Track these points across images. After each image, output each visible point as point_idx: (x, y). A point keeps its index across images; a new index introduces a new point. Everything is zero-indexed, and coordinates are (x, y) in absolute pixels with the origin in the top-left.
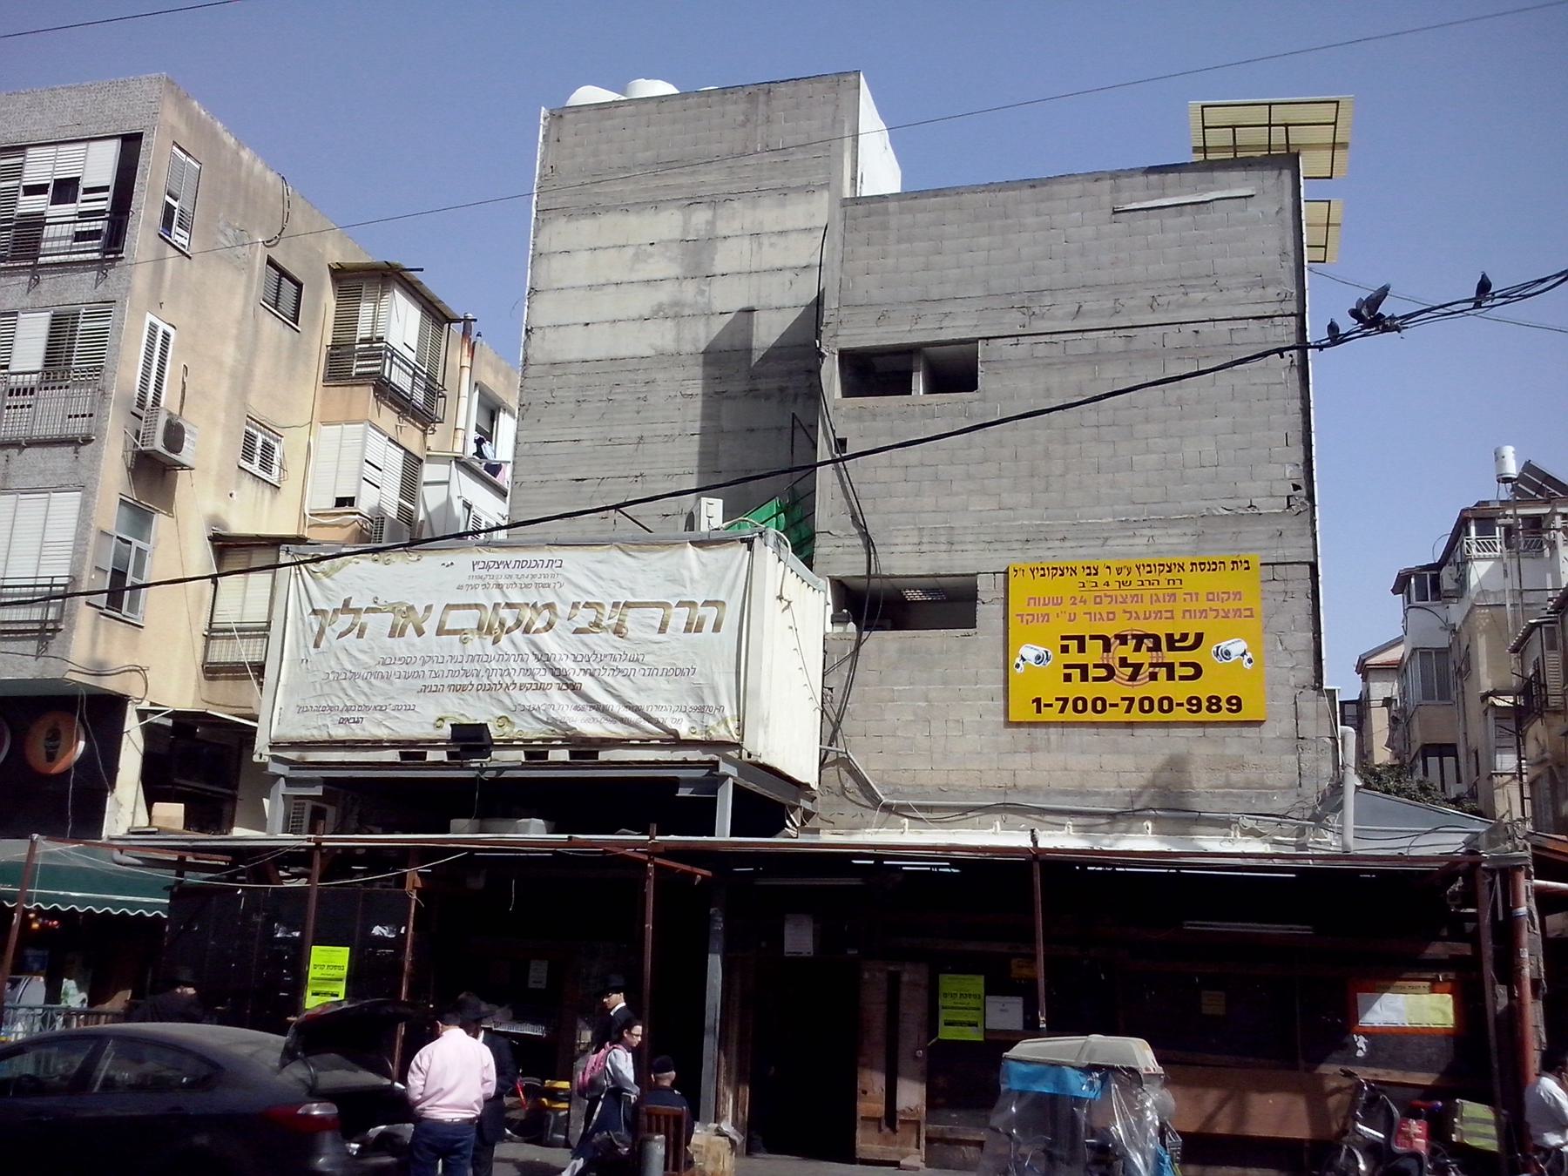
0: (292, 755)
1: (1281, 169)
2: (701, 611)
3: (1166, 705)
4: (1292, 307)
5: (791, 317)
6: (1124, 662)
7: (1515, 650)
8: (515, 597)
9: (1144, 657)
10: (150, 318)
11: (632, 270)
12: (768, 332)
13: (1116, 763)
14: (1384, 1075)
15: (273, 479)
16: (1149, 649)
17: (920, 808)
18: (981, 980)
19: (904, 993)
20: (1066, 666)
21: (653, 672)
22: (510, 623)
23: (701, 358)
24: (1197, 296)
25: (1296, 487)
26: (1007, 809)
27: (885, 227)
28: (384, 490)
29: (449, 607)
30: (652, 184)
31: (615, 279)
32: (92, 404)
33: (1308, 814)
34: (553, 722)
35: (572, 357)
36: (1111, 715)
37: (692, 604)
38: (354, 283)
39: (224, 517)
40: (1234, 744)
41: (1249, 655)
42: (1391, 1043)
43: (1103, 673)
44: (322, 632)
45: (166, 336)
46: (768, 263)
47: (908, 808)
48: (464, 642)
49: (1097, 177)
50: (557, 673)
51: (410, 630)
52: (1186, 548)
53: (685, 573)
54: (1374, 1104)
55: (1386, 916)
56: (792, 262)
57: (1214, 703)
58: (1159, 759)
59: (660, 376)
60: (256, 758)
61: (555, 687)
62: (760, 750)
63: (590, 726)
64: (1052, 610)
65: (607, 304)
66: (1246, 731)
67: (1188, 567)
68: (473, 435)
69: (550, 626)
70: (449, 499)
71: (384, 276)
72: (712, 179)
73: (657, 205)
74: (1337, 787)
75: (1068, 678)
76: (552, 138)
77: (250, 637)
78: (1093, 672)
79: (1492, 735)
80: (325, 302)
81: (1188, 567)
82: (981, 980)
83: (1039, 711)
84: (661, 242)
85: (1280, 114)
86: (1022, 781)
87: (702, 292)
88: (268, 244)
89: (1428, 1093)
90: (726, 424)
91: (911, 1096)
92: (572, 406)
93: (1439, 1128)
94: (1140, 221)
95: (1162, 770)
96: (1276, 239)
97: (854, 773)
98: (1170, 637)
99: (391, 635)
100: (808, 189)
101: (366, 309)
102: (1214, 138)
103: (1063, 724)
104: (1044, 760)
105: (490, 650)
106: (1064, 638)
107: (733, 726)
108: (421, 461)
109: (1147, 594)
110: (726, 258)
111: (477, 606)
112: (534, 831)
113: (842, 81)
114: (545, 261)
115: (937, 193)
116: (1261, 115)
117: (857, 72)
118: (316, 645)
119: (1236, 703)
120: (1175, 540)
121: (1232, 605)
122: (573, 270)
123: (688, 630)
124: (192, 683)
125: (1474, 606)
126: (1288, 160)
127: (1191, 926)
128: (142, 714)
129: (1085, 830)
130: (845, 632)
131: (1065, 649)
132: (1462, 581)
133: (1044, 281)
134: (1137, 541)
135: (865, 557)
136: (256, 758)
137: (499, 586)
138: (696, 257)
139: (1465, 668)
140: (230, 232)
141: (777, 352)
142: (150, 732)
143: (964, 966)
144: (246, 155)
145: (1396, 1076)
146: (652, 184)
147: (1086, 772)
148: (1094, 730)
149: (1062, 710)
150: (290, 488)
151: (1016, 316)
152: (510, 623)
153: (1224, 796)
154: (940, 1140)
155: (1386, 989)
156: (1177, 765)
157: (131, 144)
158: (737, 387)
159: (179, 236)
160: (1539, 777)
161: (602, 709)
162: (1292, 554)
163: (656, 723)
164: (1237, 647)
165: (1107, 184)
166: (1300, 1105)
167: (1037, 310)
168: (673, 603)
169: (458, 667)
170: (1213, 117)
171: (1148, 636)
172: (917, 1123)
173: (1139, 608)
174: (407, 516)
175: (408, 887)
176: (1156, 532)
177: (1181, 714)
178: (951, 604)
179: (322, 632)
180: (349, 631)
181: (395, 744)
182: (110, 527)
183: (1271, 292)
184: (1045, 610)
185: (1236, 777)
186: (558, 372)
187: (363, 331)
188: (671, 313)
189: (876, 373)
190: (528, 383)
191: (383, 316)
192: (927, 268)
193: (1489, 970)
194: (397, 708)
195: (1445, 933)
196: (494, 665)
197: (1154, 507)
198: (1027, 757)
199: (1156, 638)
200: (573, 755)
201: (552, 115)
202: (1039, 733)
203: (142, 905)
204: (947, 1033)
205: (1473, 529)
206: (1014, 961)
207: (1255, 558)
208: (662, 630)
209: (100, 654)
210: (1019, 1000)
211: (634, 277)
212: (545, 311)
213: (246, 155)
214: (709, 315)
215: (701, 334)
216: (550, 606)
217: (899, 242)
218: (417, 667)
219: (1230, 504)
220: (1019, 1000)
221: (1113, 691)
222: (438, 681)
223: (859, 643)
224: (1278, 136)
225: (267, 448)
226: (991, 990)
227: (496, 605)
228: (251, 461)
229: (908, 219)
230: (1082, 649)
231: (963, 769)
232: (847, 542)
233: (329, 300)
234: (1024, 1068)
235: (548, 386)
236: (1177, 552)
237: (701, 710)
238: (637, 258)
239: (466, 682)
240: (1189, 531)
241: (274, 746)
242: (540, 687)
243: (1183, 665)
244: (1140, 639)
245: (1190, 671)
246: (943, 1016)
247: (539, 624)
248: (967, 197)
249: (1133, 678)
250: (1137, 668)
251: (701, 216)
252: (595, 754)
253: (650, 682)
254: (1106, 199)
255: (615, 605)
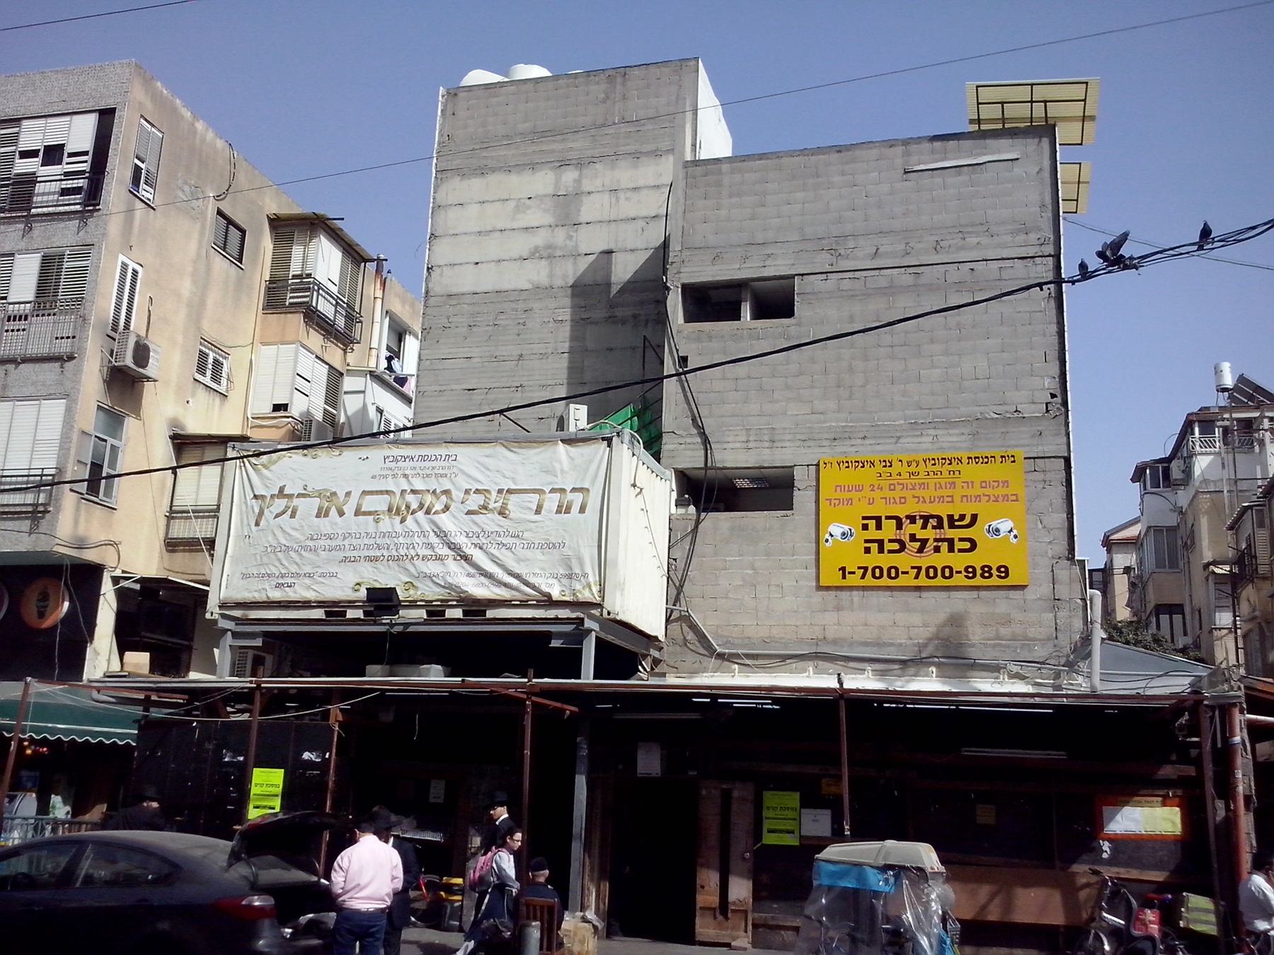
0: (237, 613)
1: (1040, 137)
2: (570, 496)
3: (947, 573)
4: (1050, 249)
5: (642, 257)
6: (913, 538)
7: (1231, 528)
8: (419, 485)
9: (930, 534)
10: (122, 258)
11: (513, 219)
12: (624, 270)
13: (906, 620)
14: (1125, 873)
15: (222, 389)
16: (934, 527)
17: (748, 656)
18: (797, 795)
19: (735, 807)
20: (866, 541)
21: (530, 546)
22: (414, 506)
23: (569, 291)
24: (973, 240)
25: (1053, 396)
26: (818, 657)
27: (719, 184)
28: (312, 398)
29: (365, 493)
30: (530, 149)
31: (499, 226)
32: (75, 328)
33: (1063, 661)
34: (449, 587)
35: (464, 290)
36: (902, 581)
37: (562, 491)
38: (287, 229)
39: (182, 419)
40: (1003, 604)
41: (1015, 532)
42: (1130, 847)
43: (896, 546)
44: (261, 513)
45: (135, 273)
46: (624, 213)
47: (737, 656)
48: (377, 521)
49: (891, 144)
50: (452, 546)
51: (333, 512)
52: (964, 445)
53: (557, 465)
54: (1116, 897)
55: (1126, 744)
56: (644, 213)
57: (986, 571)
58: (942, 616)
59: (536, 305)
60: (208, 616)
61: (451, 558)
62: (617, 609)
63: (479, 589)
64: (855, 495)
65: (493, 247)
66: (1012, 594)
67: (965, 461)
68: (384, 353)
69: (447, 508)
70: (365, 405)
71: (312, 224)
72: (578, 145)
73: (533, 167)
74: (1087, 639)
75: (867, 550)
76: (449, 112)
77: (203, 517)
78: (888, 546)
79: (1212, 597)
80: (264, 245)
81: (965, 461)
82: (797, 795)
83: (844, 577)
84: (537, 196)
85: (1040, 93)
86: (830, 634)
87: (570, 237)
88: (218, 198)
89: (1161, 887)
90: (590, 344)
91: (740, 890)
92: (465, 330)
93: (1169, 916)
94: (926, 180)
95: (944, 625)
96: (1037, 194)
97: (694, 627)
98: (950, 517)
99: (318, 516)
100: (657, 154)
101: (297, 251)
102: (986, 112)
103: (864, 588)
104: (848, 617)
105: (398, 528)
106: (864, 518)
107: (595, 589)
108: (342, 374)
109: (932, 483)
110: (590, 209)
111: (387, 492)
112: (434, 675)
113: (684, 66)
114: (442, 212)
115: (762, 156)
116: (1024, 93)
117: (696, 59)
118: (257, 524)
119: (1004, 571)
120: (954, 439)
121: (1001, 491)
122: (465, 219)
123: (559, 512)
124: (156, 555)
125: (1197, 492)
126: (1047, 130)
127: (968, 752)
128: (116, 580)
129: (882, 674)
130: (686, 514)
131: (865, 527)
132: (1188, 472)
133: (848, 229)
134: (924, 439)
135: (703, 452)
136: (208, 616)
137: (405, 476)
138: (566, 208)
139: (1191, 543)
140: (187, 188)
141: (632, 286)
142: (122, 595)
143: (784, 784)
144: (200, 126)
145: (1134, 874)
146: (530, 149)
147: (883, 627)
148: (889, 593)
149: (863, 577)
150: (236, 397)
151: (825, 257)
152: (414, 506)
153: (994, 646)
154: (763, 926)
155: (1126, 803)
156: (956, 621)
157: (106, 117)
158: (599, 314)
159: (145, 192)
160: (1250, 631)
161: (489, 576)
162: (1050, 449)
163: (533, 587)
164: (1005, 525)
165: (899, 150)
166: (1056, 897)
167: (842, 252)
168: (547, 490)
169: (372, 541)
170: (986, 95)
171: (933, 517)
172: (745, 912)
173: (926, 494)
174: (330, 419)
175: (332, 720)
176: (939, 432)
177: (959, 580)
178: (773, 490)
179: (261, 513)
180: (284, 512)
181: (321, 604)
182: (90, 428)
183: (1033, 237)
184: (849, 495)
185: (1004, 631)
186: (454, 302)
187: (295, 269)
188: (545, 254)
189: (712, 303)
190: (429, 311)
191: (311, 257)
192: (753, 218)
193: (1210, 788)
194: (323, 575)
195: (1174, 757)
196: (401, 540)
197: (938, 412)
198: (835, 614)
199: (939, 518)
200: (465, 613)
201: (448, 93)
202: (844, 595)
203: (116, 735)
204: (769, 839)
205: (1197, 430)
206: (824, 781)
207: (1020, 453)
208: (538, 512)
209: (81, 531)
210: (828, 812)
211: (515, 225)
212: (443, 252)
213: (200, 126)
214: (576, 256)
215: (570, 272)
216: (447, 492)
217: (730, 196)
218: (338, 542)
219: (999, 409)
220: (828, 812)
221: (904, 561)
222: (356, 553)
223: (698, 522)
224: (1039, 110)
225: (217, 364)
226: (805, 804)
227: (403, 492)
228: (204, 374)
229: (738, 178)
230: (879, 527)
231: (782, 625)
232: (688, 440)
233: (267, 244)
234: (832, 867)
235: (445, 314)
236: (956, 449)
237: (570, 577)
238: (517, 209)
239: (378, 553)
240: (966, 431)
241: (223, 606)
242: (439, 558)
243: (961, 540)
244: (926, 519)
245: (967, 545)
246: (767, 825)
247: (438, 507)
248: (785, 160)
249: (920, 550)
250: (924, 542)
251: (570, 176)
252: (484, 613)
253: (528, 554)
254: (899, 161)
255: (500, 491)
